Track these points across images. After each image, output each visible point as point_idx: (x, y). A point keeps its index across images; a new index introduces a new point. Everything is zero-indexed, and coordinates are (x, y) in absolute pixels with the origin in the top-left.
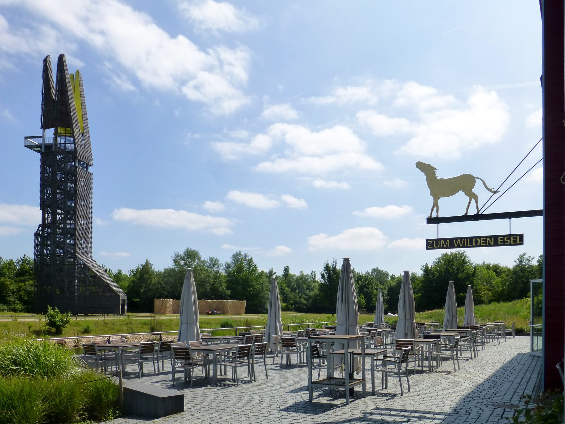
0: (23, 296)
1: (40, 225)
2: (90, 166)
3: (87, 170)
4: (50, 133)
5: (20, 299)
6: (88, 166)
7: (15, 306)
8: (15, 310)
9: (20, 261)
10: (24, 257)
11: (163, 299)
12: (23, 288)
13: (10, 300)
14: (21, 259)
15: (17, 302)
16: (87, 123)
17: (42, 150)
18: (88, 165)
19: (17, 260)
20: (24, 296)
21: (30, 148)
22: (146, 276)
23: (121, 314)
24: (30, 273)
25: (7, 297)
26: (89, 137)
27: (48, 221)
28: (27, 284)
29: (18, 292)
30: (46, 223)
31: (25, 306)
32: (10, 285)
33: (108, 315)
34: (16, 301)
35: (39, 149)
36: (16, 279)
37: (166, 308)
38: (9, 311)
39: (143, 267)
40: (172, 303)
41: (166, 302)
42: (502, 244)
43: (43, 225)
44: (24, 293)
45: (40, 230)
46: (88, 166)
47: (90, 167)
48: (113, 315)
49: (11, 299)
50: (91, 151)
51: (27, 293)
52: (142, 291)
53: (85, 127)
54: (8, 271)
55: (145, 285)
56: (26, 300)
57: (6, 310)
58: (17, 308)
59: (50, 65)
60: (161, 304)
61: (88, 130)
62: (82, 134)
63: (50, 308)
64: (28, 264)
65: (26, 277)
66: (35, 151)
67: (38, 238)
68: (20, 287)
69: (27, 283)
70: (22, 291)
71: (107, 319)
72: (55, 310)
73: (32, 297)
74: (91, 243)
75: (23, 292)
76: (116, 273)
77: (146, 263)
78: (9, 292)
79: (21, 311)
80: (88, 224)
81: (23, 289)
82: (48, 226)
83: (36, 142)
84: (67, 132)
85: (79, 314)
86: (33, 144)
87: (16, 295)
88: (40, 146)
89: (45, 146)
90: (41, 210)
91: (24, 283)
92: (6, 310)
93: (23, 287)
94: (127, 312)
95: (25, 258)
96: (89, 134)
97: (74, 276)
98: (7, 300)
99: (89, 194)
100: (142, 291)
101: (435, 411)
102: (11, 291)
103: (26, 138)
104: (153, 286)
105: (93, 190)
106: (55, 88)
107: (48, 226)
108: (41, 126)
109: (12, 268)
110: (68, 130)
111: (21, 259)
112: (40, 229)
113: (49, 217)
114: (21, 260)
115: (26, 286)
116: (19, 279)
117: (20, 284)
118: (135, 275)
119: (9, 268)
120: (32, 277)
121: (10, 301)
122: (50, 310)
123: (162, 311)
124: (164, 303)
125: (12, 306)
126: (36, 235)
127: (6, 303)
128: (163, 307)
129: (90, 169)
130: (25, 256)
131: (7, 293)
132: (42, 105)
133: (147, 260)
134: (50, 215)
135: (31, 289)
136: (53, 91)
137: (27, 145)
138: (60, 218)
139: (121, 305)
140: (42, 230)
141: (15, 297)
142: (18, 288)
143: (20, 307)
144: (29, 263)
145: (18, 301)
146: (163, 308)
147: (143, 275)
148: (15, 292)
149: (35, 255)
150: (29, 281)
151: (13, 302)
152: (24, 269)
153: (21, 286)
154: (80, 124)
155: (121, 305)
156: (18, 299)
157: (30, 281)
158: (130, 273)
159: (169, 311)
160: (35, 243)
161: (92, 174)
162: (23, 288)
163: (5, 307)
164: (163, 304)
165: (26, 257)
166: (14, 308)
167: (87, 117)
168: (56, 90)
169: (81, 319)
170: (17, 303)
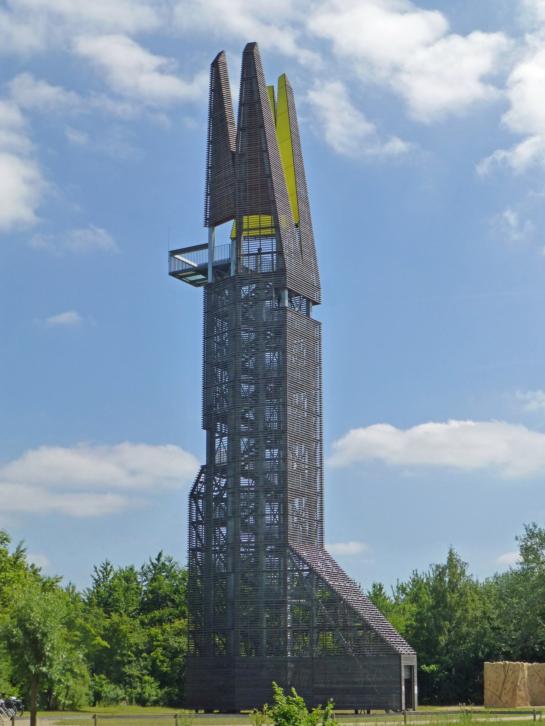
0: (160, 661)
1: (203, 469)
2: (315, 303)
3: (308, 314)
5: (154, 672)
6: (311, 304)
7: (142, 689)
8: (142, 701)
9: (150, 571)
10: (158, 559)
11: (507, 662)
12: (158, 641)
13: (131, 673)
14: (152, 564)
15: (146, 678)
16: (307, 198)
17: (207, 279)
18: (312, 302)
19: (142, 568)
20: (162, 662)
21: (181, 278)
22: (452, 598)
23: (404, 708)
24: (173, 601)
25: (124, 665)
26: (311, 231)
27: (221, 457)
28: (168, 629)
29: (149, 652)
30: (217, 461)
31: (165, 689)
32: (131, 632)
33: (369, 712)
34: (143, 675)
35: (200, 277)
36: (142, 617)
37: (514, 690)
38: (130, 702)
39: (441, 572)
40: (526, 674)
41: (515, 671)
44: (162, 655)
45: (201, 482)
46: (311, 304)
47: (314, 308)
48: (384, 712)
49: (133, 670)
50: (316, 266)
51: (169, 654)
52: (443, 640)
53: (303, 207)
54: (125, 598)
55: (451, 623)
56: (166, 672)
57: (124, 699)
58: (147, 694)
59: (226, 71)
60: (502, 673)
61: (309, 214)
62: (297, 226)
63: (279, 690)
64: (167, 577)
65: (166, 611)
66: (192, 283)
67: (197, 503)
68: (152, 638)
69: (167, 627)
70: (158, 648)
71: (412, 723)
72: (291, 698)
73: (180, 666)
74: (322, 509)
75: (160, 650)
76: (369, 593)
77: (451, 559)
78: (129, 653)
79: (156, 703)
80: (312, 457)
81: (159, 643)
82: (222, 471)
84: (263, 225)
85: (242, 712)
86: (188, 267)
87: (145, 659)
88: (202, 270)
89: (214, 268)
90: (204, 428)
91: (161, 625)
92: (124, 699)
93: (161, 637)
94: (420, 704)
95: (161, 562)
96: (310, 225)
97: (285, 603)
98: (124, 673)
99: (315, 377)
100: (443, 640)
102: (134, 649)
103: (173, 253)
104: (471, 624)
105: (323, 366)
106: (236, 124)
107: (222, 471)
108: (206, 219)
109: (133, 589)
110: (267, 220)
111: (152, 564)
112: (202, 479)
114: (151, 567)
115: (166, 634)
116: (149, 616)
117: (154, 631)
118: (415, 599)
119: (127, 589)
120: (178, 612)
121: (130, 676)
122: (280, 697)
123: (505, 698)
124: (510, 673)
125: (135, 688)
126: (194, 496)
127: (121, 682)
128: (508, 686)
129: (315, 312)
130: (160, 555)
131: (125, 655)
132: (208, 168)
133: (451, 553)
134: (225, 439)
135: (183, 642)
136: (233, 130)
137: (172, 271)
138: (246, 447)
139: (403, 683)
140: (208, 482)
141: (142, 664)
142: (149, 642)
143: (154, 693)
144: (171, 576)
145: (148, 675)
146: (508, 689)
147: (444, 597)
148: (142, 652)
149: (190, 549)
150: (173, 620)
151: (138, 677)
152: (160, 589)
153: (156, 636)
154: (292, 201)
155: (403, 683)
156: (148, 670)
157: (173, 622)
158: (396, 594)
159: (521, 698)
160: (190, 518)
161: (320, 324)
162: (158, 641)
163: (121, 692)
164: (508, 679)
165: (163, 559)
166: (140, 694)
167: (305, 184)
168: (239, 129)
170: (146, 682)
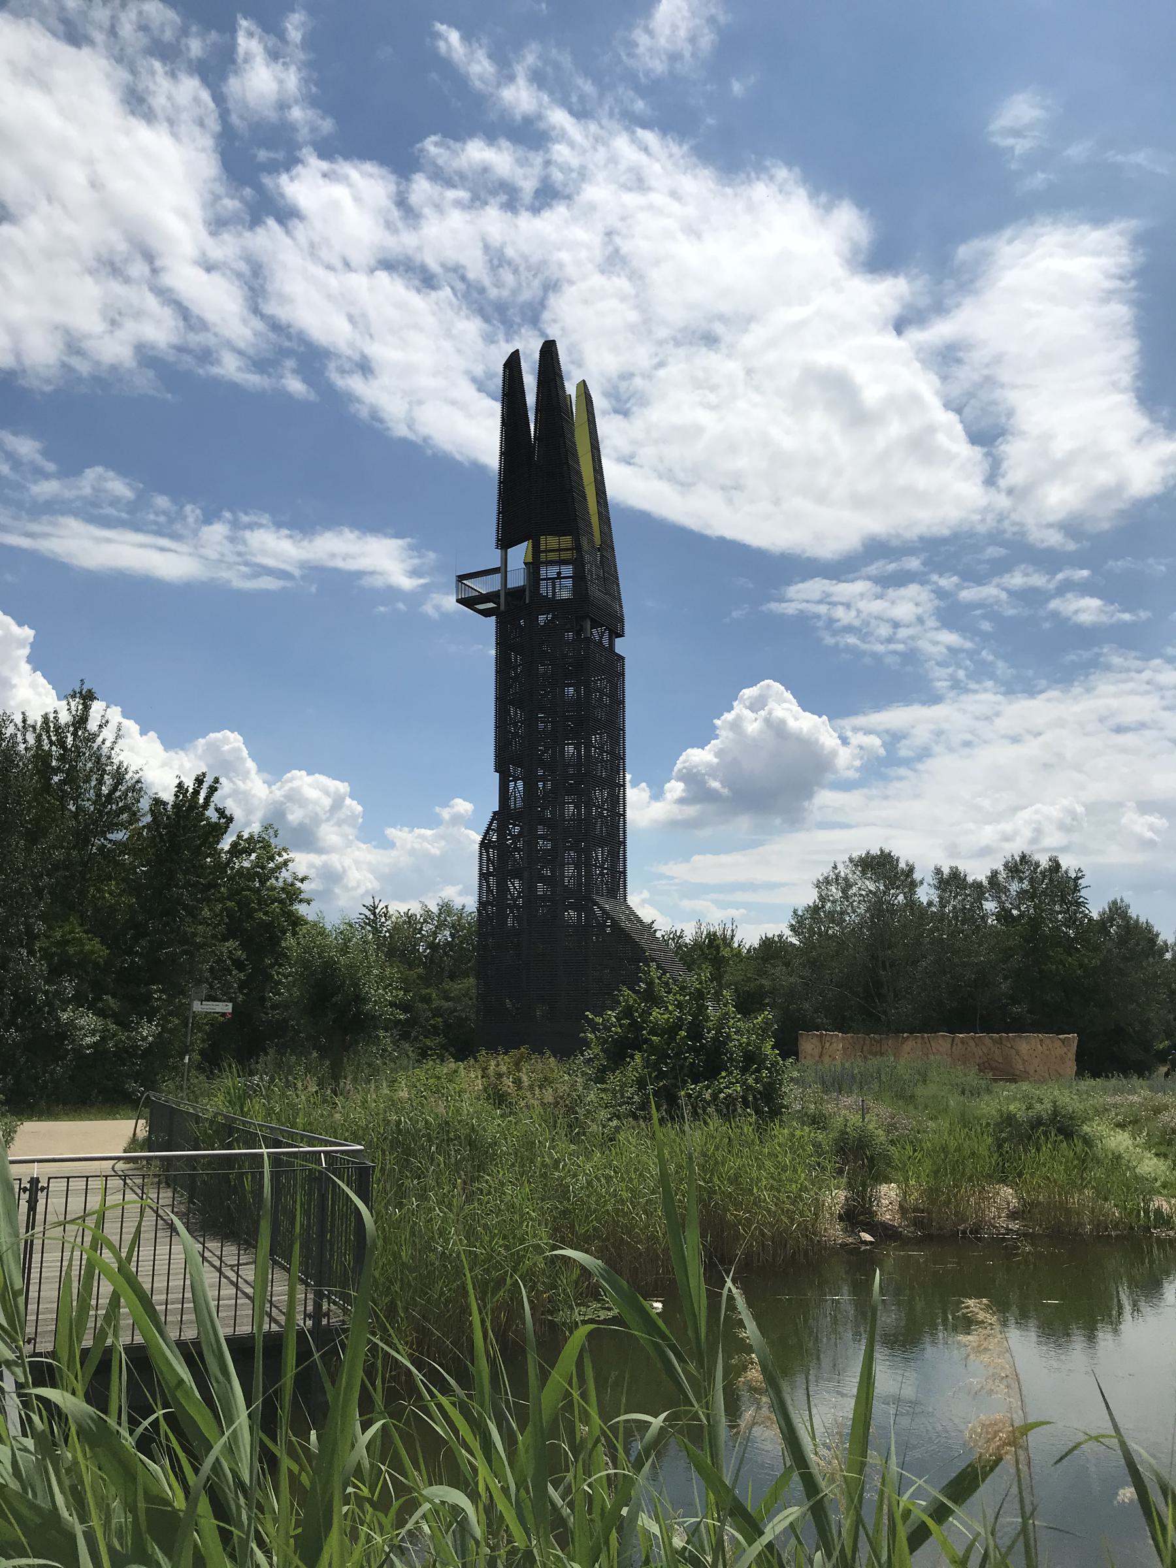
4: (519, 554)
27: (517, 803)
35: (491, 605)
42: (878, 1271)
43: (502, 818)
47: (618, 641)
67: (488, 852)
82: (518, 817)
83: (482, 586)
101: (777, 1532)
103: (461, 578)
107: (518, 817)
108: (498, 540)
113: (518, 787)
134: (520, 784)
160: (481, 869)
169: (858, 642)
